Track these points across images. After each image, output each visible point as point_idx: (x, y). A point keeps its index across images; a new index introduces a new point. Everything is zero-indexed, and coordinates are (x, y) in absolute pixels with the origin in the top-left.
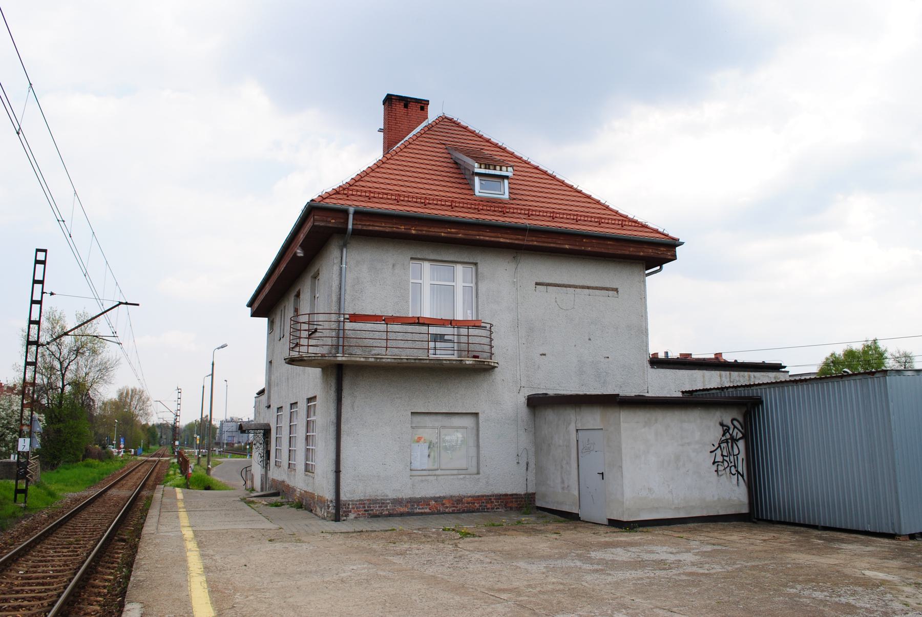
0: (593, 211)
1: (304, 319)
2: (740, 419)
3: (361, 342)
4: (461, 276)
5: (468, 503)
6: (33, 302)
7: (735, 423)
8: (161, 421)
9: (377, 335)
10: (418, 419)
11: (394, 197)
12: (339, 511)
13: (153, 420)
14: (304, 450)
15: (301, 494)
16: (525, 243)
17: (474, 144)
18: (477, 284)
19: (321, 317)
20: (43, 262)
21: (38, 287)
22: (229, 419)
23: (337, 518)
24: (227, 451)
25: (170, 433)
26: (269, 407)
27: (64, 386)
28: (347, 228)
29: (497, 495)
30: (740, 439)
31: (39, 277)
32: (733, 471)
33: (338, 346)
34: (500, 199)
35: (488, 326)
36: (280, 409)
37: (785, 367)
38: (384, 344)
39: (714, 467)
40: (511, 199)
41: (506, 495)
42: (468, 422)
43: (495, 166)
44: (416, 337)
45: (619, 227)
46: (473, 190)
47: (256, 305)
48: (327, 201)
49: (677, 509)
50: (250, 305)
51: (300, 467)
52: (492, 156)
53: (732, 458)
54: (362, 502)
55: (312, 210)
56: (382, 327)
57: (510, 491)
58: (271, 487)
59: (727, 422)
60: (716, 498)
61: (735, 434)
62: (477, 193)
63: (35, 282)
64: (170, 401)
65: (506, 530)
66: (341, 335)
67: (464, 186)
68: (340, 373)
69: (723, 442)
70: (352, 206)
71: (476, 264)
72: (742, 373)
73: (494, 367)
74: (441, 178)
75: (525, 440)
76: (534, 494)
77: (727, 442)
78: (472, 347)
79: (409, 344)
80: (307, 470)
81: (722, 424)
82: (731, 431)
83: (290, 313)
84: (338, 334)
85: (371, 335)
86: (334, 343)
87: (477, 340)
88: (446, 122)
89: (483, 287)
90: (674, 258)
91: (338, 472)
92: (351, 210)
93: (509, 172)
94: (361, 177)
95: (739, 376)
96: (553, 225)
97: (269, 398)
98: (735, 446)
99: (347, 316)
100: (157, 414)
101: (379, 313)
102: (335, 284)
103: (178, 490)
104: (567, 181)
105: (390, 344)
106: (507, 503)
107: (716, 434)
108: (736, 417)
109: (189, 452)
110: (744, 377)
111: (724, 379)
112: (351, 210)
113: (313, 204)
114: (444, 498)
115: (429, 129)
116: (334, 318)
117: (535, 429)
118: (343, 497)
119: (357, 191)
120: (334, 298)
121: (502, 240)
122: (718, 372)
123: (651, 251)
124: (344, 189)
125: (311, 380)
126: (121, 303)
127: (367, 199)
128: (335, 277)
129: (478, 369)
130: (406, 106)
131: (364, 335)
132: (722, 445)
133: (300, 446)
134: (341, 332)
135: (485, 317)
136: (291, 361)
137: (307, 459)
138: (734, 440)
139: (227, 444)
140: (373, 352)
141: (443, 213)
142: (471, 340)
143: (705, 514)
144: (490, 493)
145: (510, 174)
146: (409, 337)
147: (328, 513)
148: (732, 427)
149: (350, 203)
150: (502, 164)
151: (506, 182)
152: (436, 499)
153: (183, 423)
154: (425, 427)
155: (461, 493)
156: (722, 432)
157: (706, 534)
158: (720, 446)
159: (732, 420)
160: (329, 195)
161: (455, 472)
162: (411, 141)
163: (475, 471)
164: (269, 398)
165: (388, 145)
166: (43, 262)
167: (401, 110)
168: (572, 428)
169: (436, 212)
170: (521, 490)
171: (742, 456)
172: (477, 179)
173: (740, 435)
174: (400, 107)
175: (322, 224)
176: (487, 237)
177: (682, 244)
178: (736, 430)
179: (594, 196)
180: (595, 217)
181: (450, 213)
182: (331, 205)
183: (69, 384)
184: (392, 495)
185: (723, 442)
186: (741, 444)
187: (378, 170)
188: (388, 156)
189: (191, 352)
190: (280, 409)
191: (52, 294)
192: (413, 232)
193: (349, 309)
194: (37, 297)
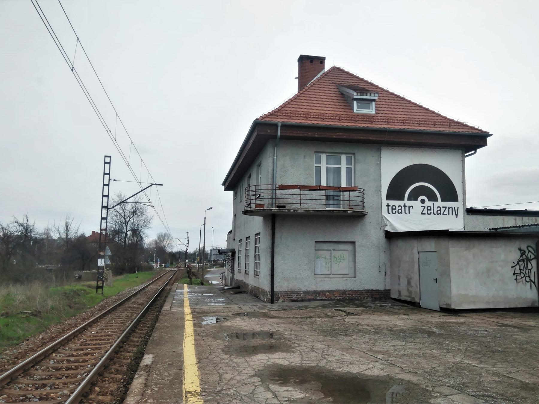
0: (430, 118)
1: (253, 188)
2: (534, 246)
5: (349, 294)
6: (104, 185)
7: (530, 249)
8: (179, 250)
9: (295, 197)
10: (319, 245)
12: (273, 297)
13: (175, 250)
14: (253, 263)
15: (252, 288)
16: (386, 139)
17: (352, 83)
18: (354, 166)
19: (263, 187)
20: (109, 163)
21: (107, 177)
22: (215, 248)
23: (272, 302)
24: (213, 265)
25: (184, 257)
26: (234, 240)
27: (127, 231)
28: (277, 135)
30: (533, 259)
31: (107, 171)
32: (528, 279)
33: (272, 203)
35: (362, 190)
36: (240, 240)
38: (299, 202)
39: (514, 277)
40: (376, 113)
41: (372, 290)
42: (349, 247)
43: (367, 94)
44: (318, 197)
45: (448, 126)
46: (352, 109)
47: (227, 184)
49: (488, 303)
50: (224, 184)
51: (251, 272)
52: (364, 88)
53: (527, 271)
54: (286, 292)
55: (258, 125)
56: (298, 192)
57: (375, 288)
58: (236, 283)
59: (524, 247)
60: (515, 297)
61: (529, 256)
62: (355, 111)
63: (105, 174)
64: (183, 239)
65: (373, 311)
66: (274, 197)
67: (346, 108)
69: (520, 261)
70: (280, 121)
71: (354, 154)
72: (530, 218)
74: (333, 103)
75: (383, 258)
76: (390, 290)
77: (524, 261)
78: (351, 203)
79: (314, 202)
80: (255, 274)
81: (520, 249)
82: (526, 254)
83: (245, 185)
84: (272, 196)
85: (291, 197)
87: (355, 199)
88: (336, 70)
90: (485, 144)
91: (272, 275)
92: (280, 124)
93: (375, 97)
94: (285, 105)
95: (529, 219)
97: (234, 235)
98: (529, 263)
99: (278, 186)
100: (176, 246)
101: (296, 184)
102: (270, 169)
103: (186, 285)
105: (303, 201)
106: (373, 295)
107: (515, 255)
108: (529, 245)
109: (191, 266)
110: (532, 220)
111: (517, 221)
112: (280, 124)
114: (335, 291)
116: (270, 187)
117: (389, 251)
118: (276, 290)
120: (270, 176)
121: (371, 138)
122: (514, 217)
123: (472, 140)
124: (279, 110)
125: (257, 223)
127: (289, 117)
128: (271, 165)
130: (311, 62)
131: (287, 197)
132: (520, 263)
133: (251, 261)
134: (274, 195)
135: (359, 184)
136: (245, 213)
137: (255, 268)
138: (529, 260)
139: (214, 261)
140: (293, 207)
142: (351, 199)
143: (507, 306)
144: (362, 289)
146: (314, 197)
147: (267, 298)
148: (527, 251)
150: (371, 92)
151: (374, 103)
152: (329, 291)
153: (191, 250)
154: (323, 250)
155: (345, 289)
156: (520, 255)
157: (510, 320)
158: (518, 263)
159: (527, 247)
160: (266, 116)
161: (341, 276)
162: (315, 82)
163: (353, 276)
165: (301, 86)
166: (109, 163)
167: (309, 65)
168: (415, 251)
170: (381, 287)
171: (534, 270)
172: (355, 103)
173: (533, 257)
174: (308, 63)
175: (263, 133)
176: (362, 137)
177: (491, 135)
178: (530, 254)
179: (430, 109)
180: (431, 122)
183: (130, 230)
184: (304, 289)
185: (520, 261)
186: (534, 262)
188: (301, 92)
190: (240, 240)
191: (114, 180)
192: (316, 136)
193: (279, 182)
194: (106, 182)
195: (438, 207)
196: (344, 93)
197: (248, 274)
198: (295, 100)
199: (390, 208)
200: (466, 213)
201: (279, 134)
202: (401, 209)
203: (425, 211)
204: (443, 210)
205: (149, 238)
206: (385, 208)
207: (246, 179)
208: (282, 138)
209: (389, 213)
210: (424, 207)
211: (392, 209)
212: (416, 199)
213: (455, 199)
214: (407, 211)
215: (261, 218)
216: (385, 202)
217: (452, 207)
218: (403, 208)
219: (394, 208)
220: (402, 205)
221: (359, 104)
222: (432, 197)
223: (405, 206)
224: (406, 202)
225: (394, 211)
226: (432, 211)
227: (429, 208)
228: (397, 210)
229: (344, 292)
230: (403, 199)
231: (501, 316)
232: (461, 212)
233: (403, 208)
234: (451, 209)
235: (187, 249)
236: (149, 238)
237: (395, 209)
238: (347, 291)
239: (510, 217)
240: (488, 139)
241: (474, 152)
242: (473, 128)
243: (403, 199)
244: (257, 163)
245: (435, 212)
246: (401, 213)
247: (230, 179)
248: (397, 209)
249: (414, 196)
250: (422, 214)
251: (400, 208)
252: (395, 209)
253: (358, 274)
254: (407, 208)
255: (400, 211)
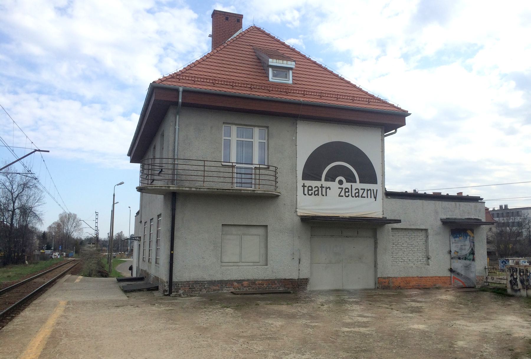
3: (189, 178)
4: (257, 136)
5: (259, 284)
10: (226, 229)
11: (318, 94)
18: (268, 140)
28: (178, 102)
29: (278, 280)
34: (286, 84)
35: (274, 169)
37: (482, 199)
38: (201, 178)
40: (294, 83)
41: (285, 279)
42: (261, 231)
46: (268, 77)
47: (132, 155)
48: (164, 83)
50: (129, 154)
51: (153, 261)
62: (270, 79)
68: (174, 198)
71: (268, 127)
73: (278, 196)
80: (156, 263)
86: (171, 178)
88: (255, 30)
89: (272, 143)
90: (403, 124)
92: (181, 89)
93: (291, 64)
96: (233, 91)
97: (141, 216)
100: (84, 232)
104: (334, 72)
112: (181, 89)
113: (155, 85)
115: (243, 35)
118: (175, 279)
119: (224, 82)
122: (433, 202)
123: (390, 119)
124: (177, 75)
126: (36, 150)
129: (269, 198)
135: (273, 162)
137: (157, 256)
140: (197, 185)
141: (245, 92)
144: (274, 278)
145: (293, 67)
146: (221, 175)
149: (181, 84)
151: (291, 72)
152: (239, 282)
161: (251, 264)
164: (141, 216)
169: (240, 92)
177: (410, 114)
181: (230, 90)
182: (167, 86)
184: (208, 278)
187: (203, 63)
189: (92, 187)
195: (315, 188)
196: (260, 58)
197: (151, 263)
198: (203, 63)
199: (306, 189)
200: (385, 196)
201: (180, 101)
202: (318, 190)
203: (343, 193)
204: (361, 192)
205: (46, 220)
206: (300, 190)
207: (152, 149)
208: (185, 105)
209: (305, 195)
210: (342, 188)
211: (308, 190)
212: (333, 180)
213: (374, 180)
214: (324, 193)
215: (162, 197)
216: (300, 182)
217: (370, 190)
218: (320, 189)
219: (310, 188)
220: (319, 186)
221: (275, 72)
222: (351, 179)
223: (322, 187)
224: (323, 182)
225: (310, 192)
226: (350, 193)
227: (347, 190)
228: (313, 192)
229: (253, 282)
230: (320, 180)
231: (485, 318)
232: (380, 195)
233: (320, 189)
234: (369, 192)
235: (97, 234)
236: (46, 220)
237: (312, 190)
238: (257, 280)
239: (430, 202)
240: (407, 119)
241: (394, 131)
242: (393, 106)
243: (320, 180)
244: (160, 133)
245: (353, 195)
246: (318, 194)
247: (135, 149)
248: (314, 190)
249: (331, 177)
250: (339, 196)
251: (317, 189)
252: (312, 190)
253: (270, 262)
254: (324, 190)
255: (316, 193)
